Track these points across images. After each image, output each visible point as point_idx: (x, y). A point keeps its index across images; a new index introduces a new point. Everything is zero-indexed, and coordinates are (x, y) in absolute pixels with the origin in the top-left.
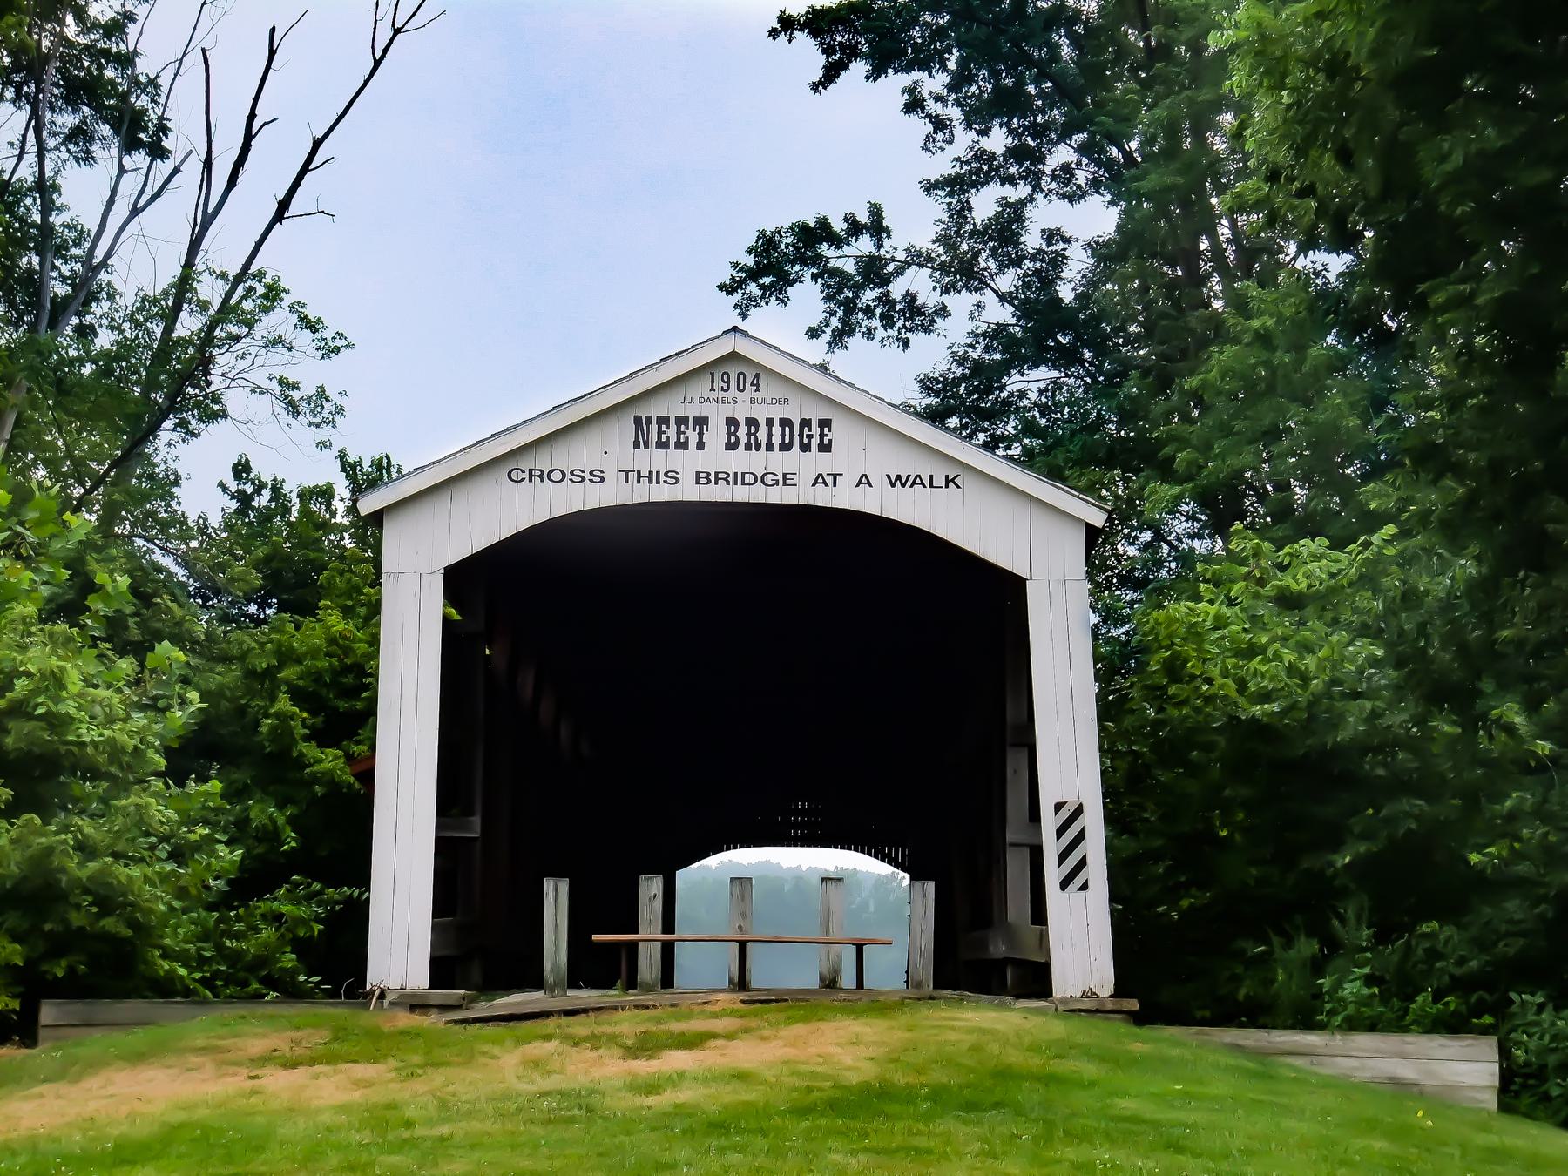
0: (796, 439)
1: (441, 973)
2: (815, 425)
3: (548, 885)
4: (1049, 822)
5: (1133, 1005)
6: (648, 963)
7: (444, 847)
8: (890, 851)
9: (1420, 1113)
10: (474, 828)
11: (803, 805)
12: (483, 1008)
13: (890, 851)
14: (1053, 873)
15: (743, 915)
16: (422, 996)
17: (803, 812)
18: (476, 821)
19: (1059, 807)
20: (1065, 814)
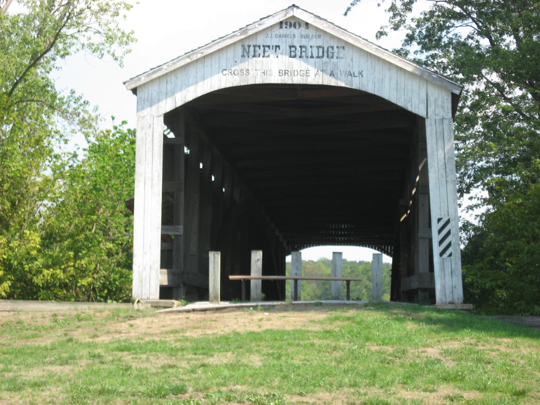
0: (325, 54)
1: (392, 299)
2: (335, 48)
3: (211, 255)
4: (435, 227)
5: (470, 306)
6: (289, 288)
7: (165, 238)
8: (385, 247)
9: (510, 3)
10: (180, 229)
11: (344, 226)
12: (191, 306)
13: (385, 247)
14: (437, 250)
15: (297, 269)
16: (157, 302)
17: (344, 229)
18: (181, 227)
19: (439, 220)
20: (442, 223)
